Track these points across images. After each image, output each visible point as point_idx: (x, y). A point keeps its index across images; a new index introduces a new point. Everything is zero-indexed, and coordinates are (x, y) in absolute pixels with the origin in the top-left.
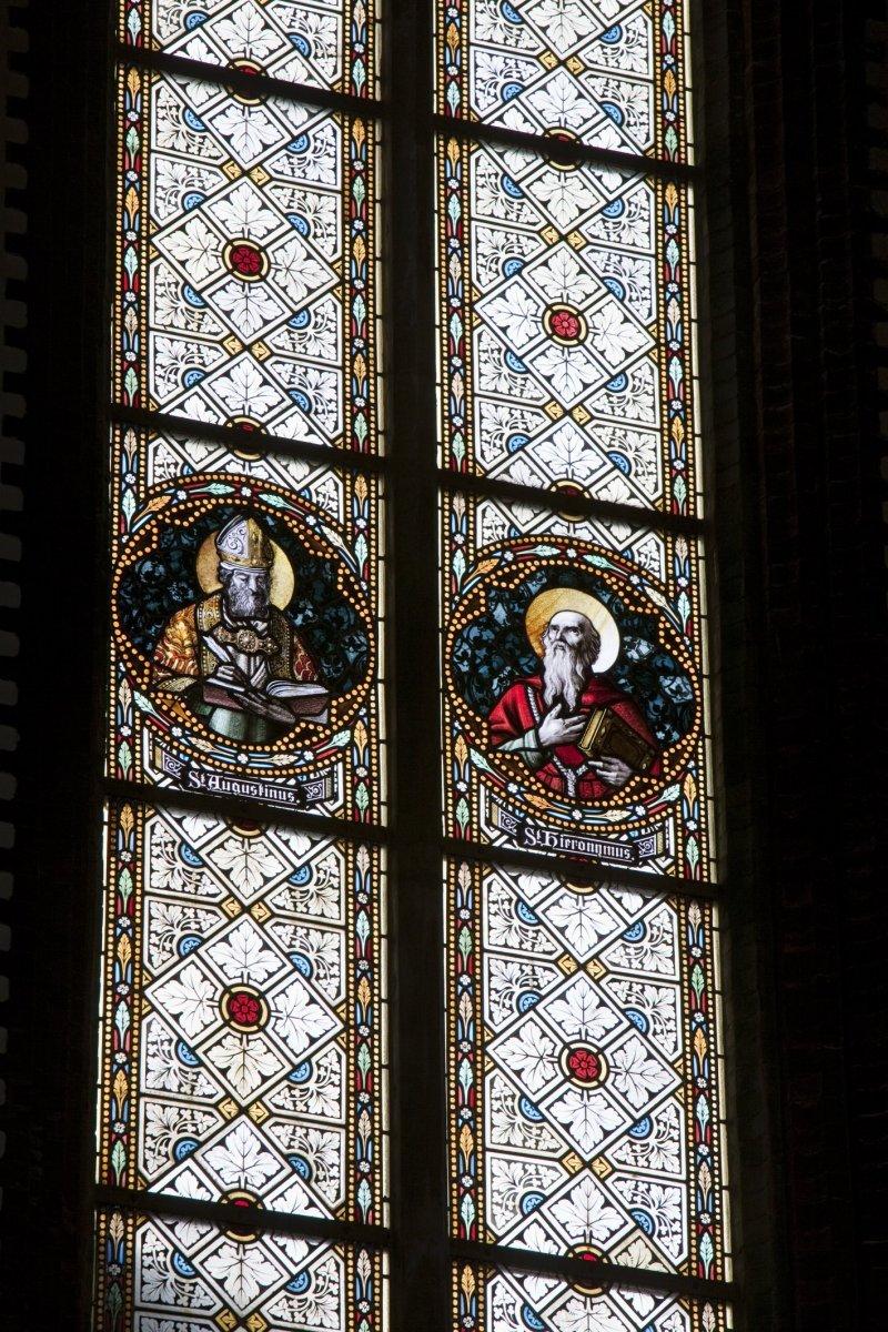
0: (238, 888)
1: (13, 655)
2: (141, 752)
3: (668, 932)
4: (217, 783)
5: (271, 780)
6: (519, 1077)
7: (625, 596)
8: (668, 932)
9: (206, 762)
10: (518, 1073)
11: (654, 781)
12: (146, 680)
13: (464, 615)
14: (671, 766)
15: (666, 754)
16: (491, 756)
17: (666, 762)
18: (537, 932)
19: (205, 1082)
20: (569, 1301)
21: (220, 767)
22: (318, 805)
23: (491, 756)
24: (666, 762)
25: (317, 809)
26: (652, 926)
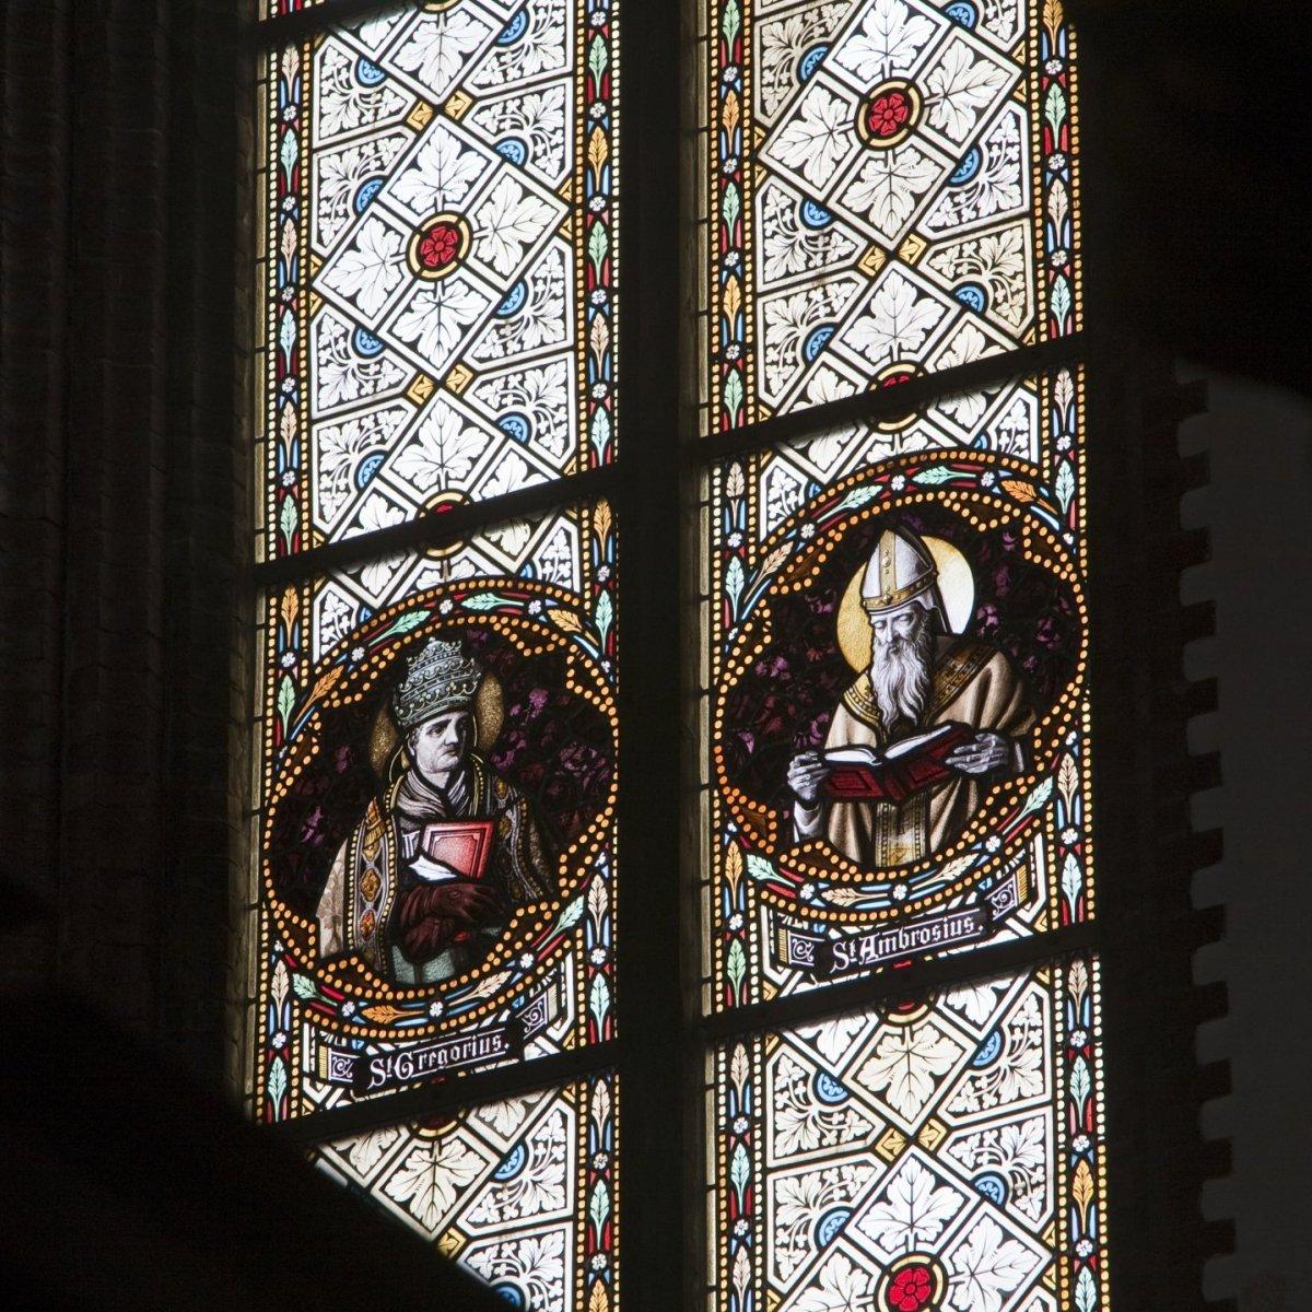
0: (1027, 1275)
1: (428, 965)
2: (759, 942)
3: (839, 1137)
4: (872, 948)
5: (942, 908)
6: (470, 327)
7: (751, 653)
8: (839, 1137)
9: (848, 923)
10: (465, 329)
11: (1026, 531)
12: (792, 863)
13: (367, 986)
14: (999, 513)
15: (982, 527)
16: (565, 893)
17: (994, 524)
18: (807, 1248)
19: (338, 503)
20: (844, 101)
21: (868, 922)
22: (1011, 922)
23: (565, 893)
24: (994, 524)
25: (1009, 928)
26: (845, 1111)
